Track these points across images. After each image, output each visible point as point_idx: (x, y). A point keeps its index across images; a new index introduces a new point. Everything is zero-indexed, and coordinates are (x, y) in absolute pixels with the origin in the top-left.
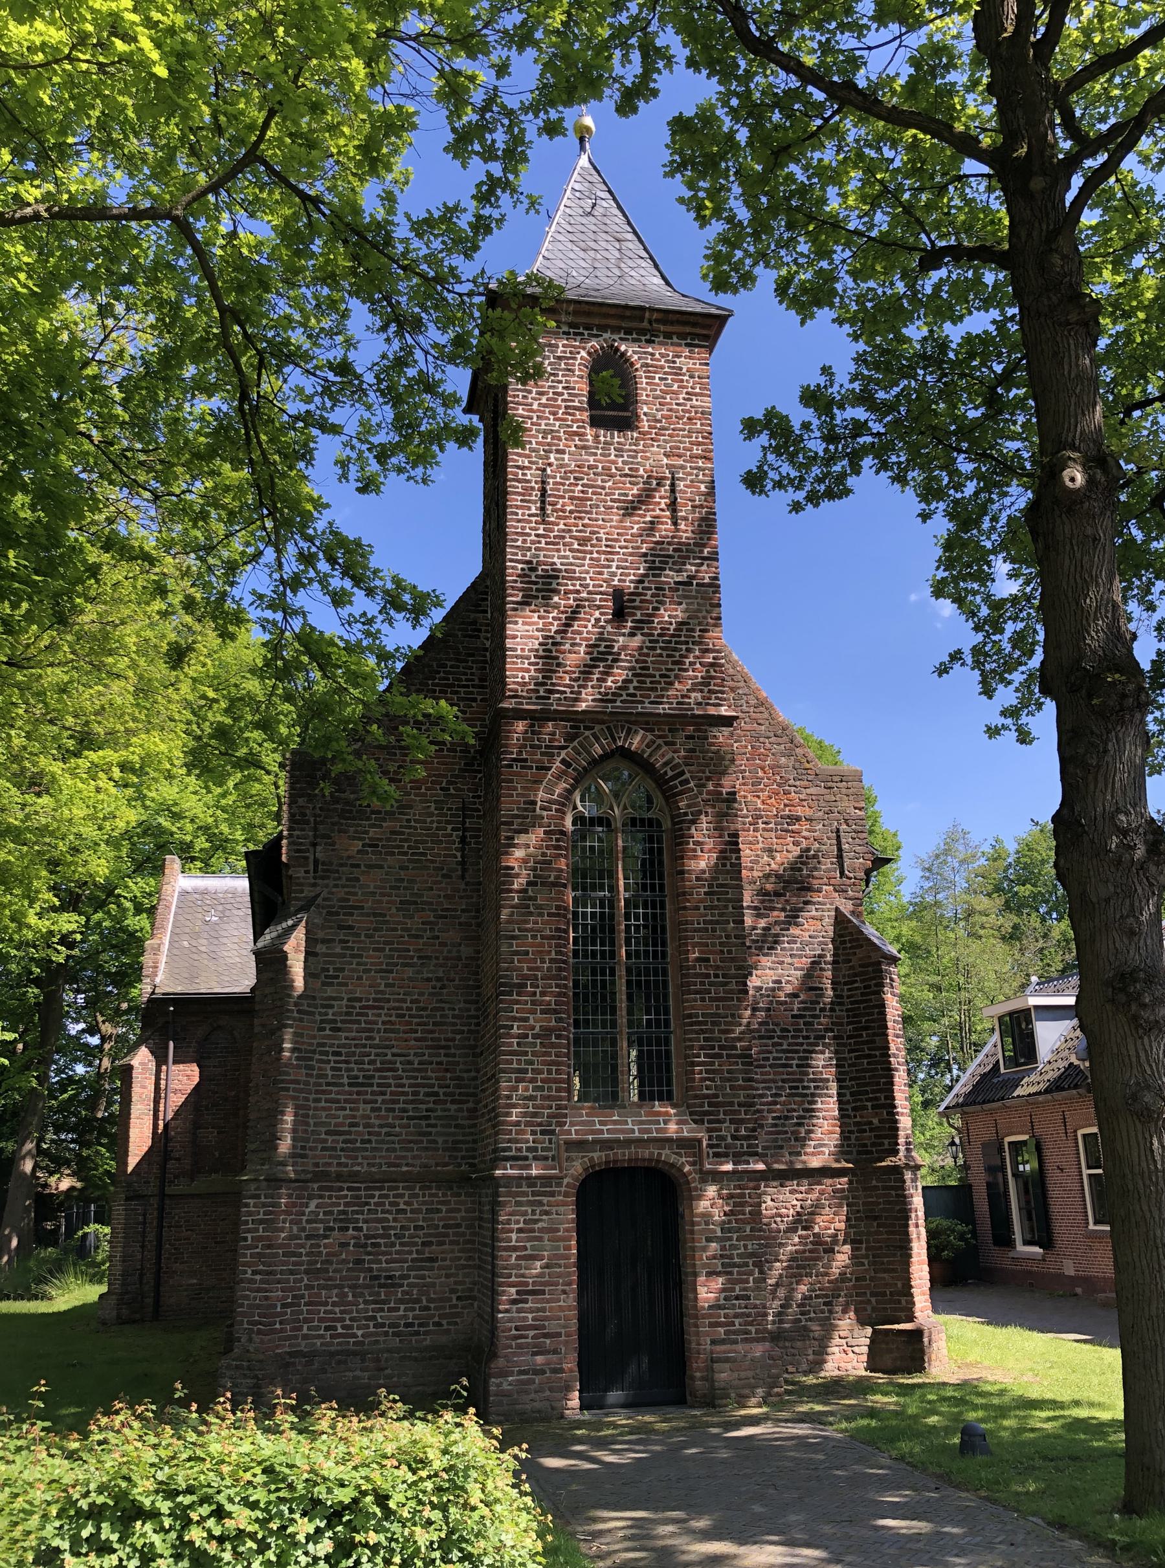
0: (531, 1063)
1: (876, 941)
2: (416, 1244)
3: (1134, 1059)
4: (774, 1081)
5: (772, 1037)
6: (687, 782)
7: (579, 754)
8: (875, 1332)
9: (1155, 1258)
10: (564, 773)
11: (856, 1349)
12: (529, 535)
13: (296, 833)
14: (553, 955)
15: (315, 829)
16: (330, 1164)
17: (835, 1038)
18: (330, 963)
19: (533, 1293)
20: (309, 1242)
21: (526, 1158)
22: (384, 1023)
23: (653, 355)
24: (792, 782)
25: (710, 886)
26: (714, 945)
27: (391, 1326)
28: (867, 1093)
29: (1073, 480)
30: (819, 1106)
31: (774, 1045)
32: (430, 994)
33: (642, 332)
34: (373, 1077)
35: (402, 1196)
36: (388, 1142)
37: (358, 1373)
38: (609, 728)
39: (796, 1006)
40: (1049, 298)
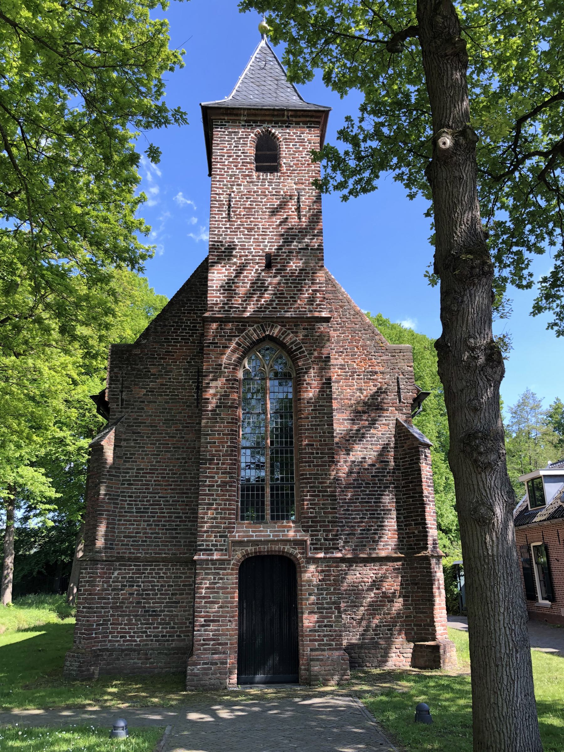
0: (216, 500)
1: (417, 436)
2: (168, 594)
3: (476, 487)
4: (361, 511)
5: (360, 487)
6: (303, 352)
7: (245, 339)
8: (415, 645)
9: (486, 610)
10: (237, 349)
11: (405, 655)
12: (221, 228)
13: (113, 386)
14: (229, 444)
15: (122, 384)
16: (125, 553)
17: (395, 487)
18: (128, 451)
19: (213, 621)
20: (113, 593)
21: (211, 550)
22: (155, 481)
23: (289, 133)
24: (373, 354)
25: (315, 406)
26: (316, 437)
27: (154, 636)
28: (412, 516)
29: (444, 143)
30: (386, 524)
31: (361, 491)
32: (179, 466)
33: (284, 122)
34: (148, 508)
35: (162, 569)
36: (155, 542)
37: (136, 661)
38: (262, 326)
39: (374, 471)
40: (435, 42)
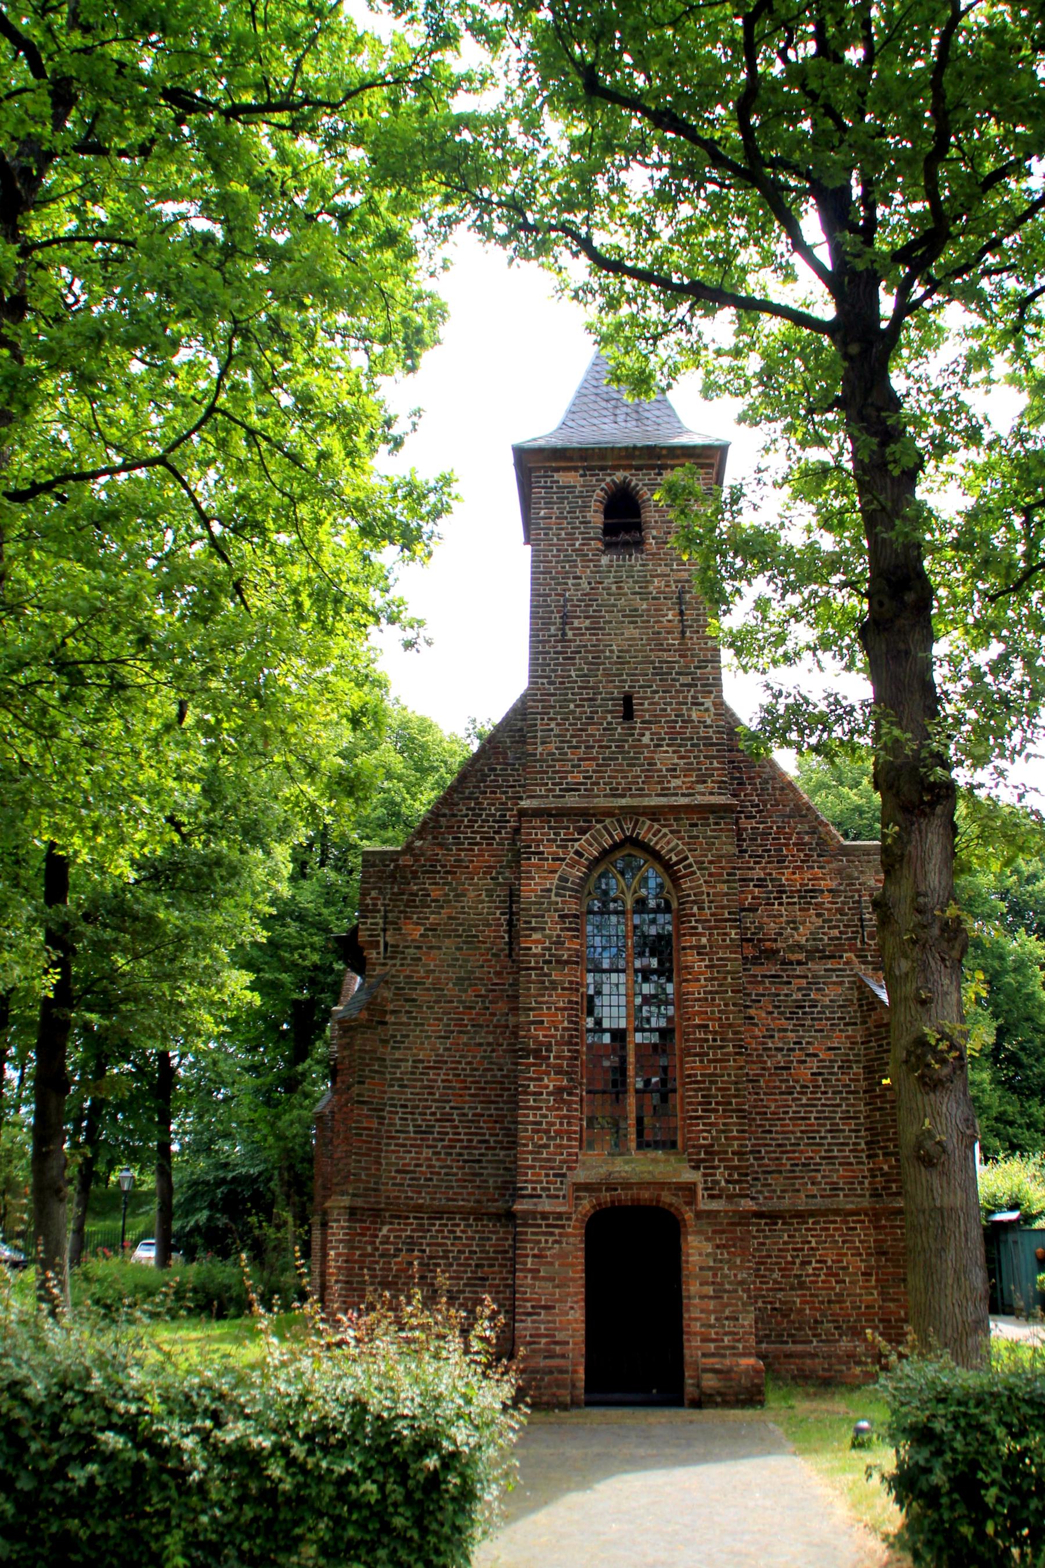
15: (385, 917)
